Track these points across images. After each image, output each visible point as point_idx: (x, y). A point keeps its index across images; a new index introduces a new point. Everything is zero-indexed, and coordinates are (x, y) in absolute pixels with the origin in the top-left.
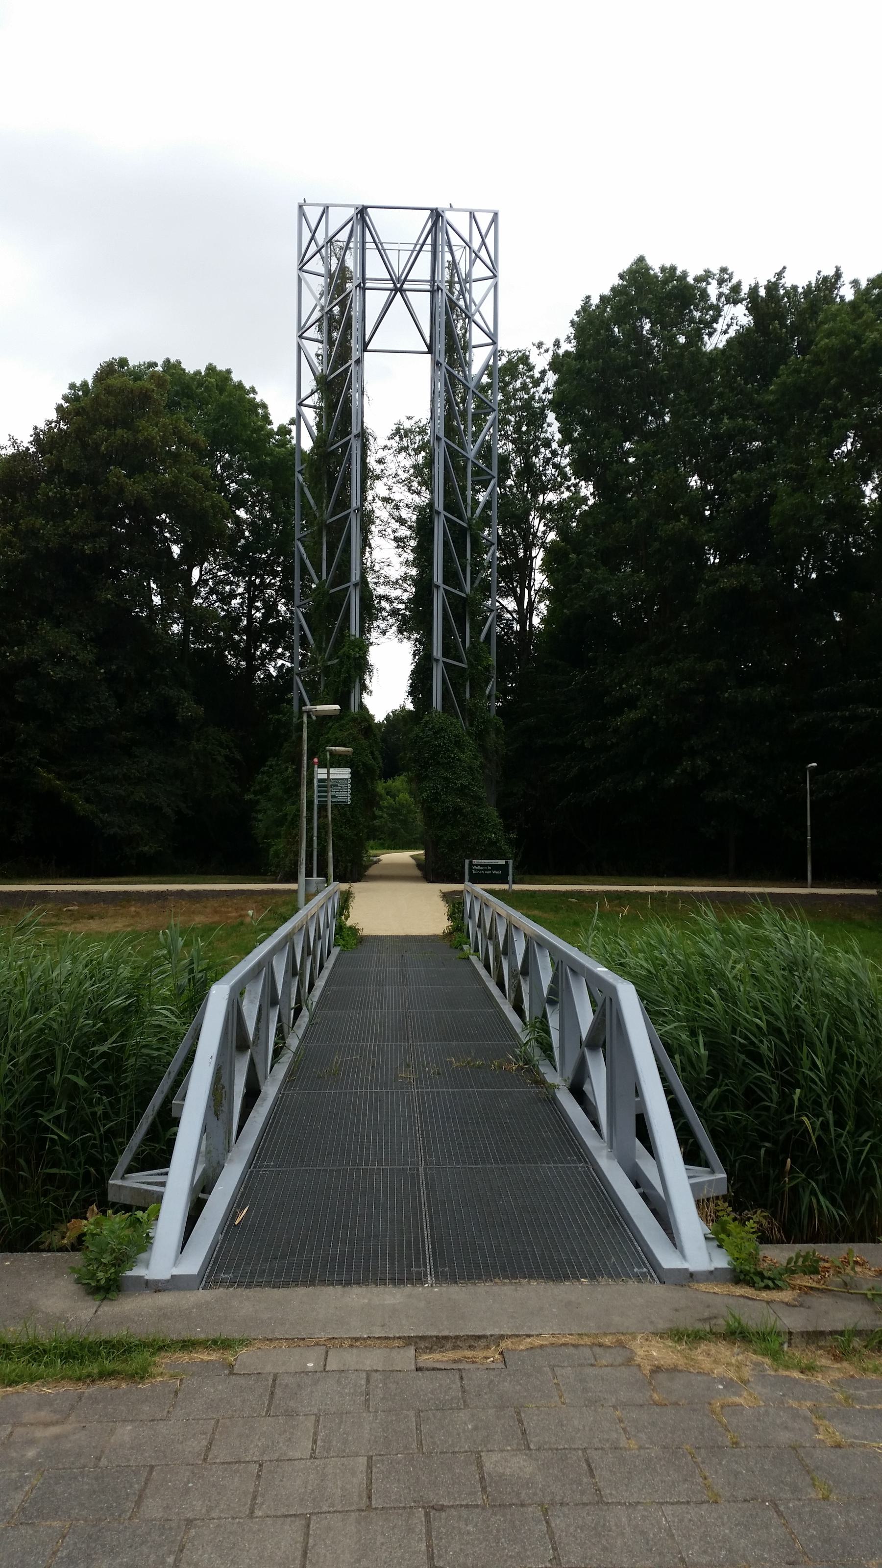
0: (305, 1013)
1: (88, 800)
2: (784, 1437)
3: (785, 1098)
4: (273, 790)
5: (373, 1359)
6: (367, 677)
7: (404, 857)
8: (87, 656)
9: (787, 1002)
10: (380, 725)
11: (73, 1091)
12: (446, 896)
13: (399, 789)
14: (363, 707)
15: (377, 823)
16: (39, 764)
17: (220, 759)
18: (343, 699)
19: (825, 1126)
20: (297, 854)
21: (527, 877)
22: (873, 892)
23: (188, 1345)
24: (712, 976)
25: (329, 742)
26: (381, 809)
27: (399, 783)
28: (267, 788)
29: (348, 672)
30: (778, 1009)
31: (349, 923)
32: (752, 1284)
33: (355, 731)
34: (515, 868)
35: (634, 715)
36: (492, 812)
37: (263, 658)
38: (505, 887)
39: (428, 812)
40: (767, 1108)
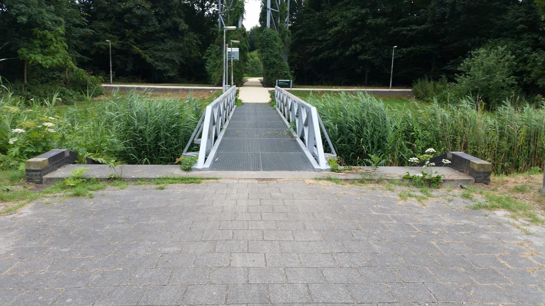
0: (227, 121)
1: (150, 57)
2: (334, 192)
3: (358, 141)
4: (213, 55)
5: (250, 181)
6: (244, 15)
7: (257, 80)
8: (148, 6)
9: (361, 115)
10: (248, 32)
11: (166, 137)
12: (270, 92)
13: (255, 56)
14: (243, 26)
15: (247, 67)
16: (134, 44)
17: (194, 44)
18: (236, 24)
19: (368, 148)
20: (222, 77)
21: (297, 86)
22: (410, 90)
23: (208, 179)
24: (342, 109)
25: (231, 39)
26: (248, 62)
27: (255, 53)
28: (210, 54)
29: (238, 13)
30: (358, 117)
31: (239, 98)
32: (335, 172)
33: (240, 35)
34: (293, 83)
35: (337, 29)
36: (286, 64)
37: (207, 7)
38: (289, 89)
39: (265, 64)
40: (353, 144)
